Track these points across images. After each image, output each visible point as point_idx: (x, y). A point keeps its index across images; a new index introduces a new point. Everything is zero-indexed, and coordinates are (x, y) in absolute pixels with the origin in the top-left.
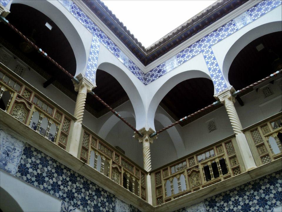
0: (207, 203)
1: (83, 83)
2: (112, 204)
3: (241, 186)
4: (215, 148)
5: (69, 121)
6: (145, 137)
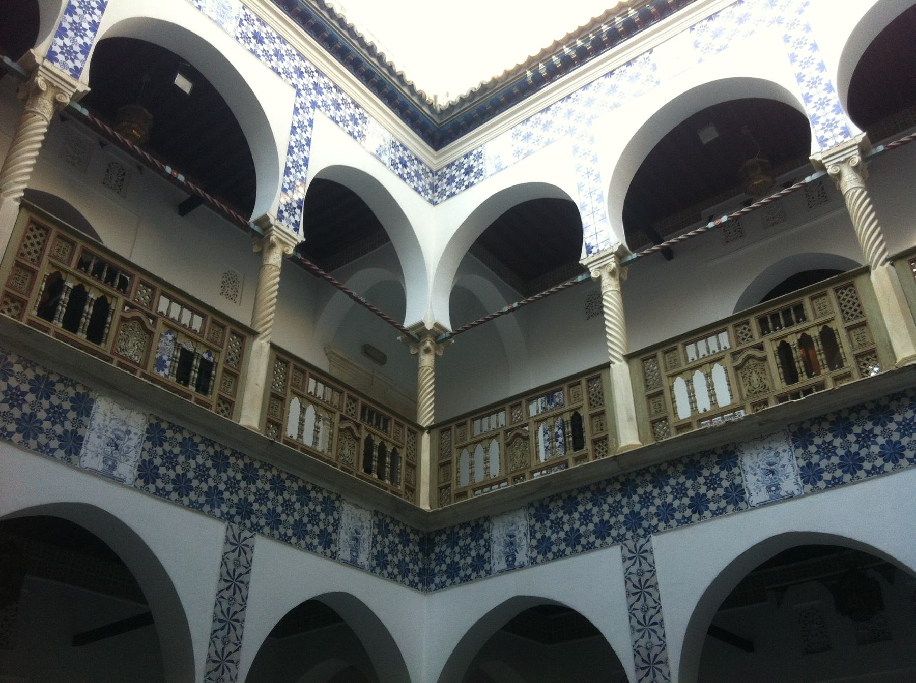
0: (533, 511)
1: (271, 238)
2: (334, 515)
3: (600, 483)
4: (566, 389)
5: (242, 339)
6: (425, 343)
